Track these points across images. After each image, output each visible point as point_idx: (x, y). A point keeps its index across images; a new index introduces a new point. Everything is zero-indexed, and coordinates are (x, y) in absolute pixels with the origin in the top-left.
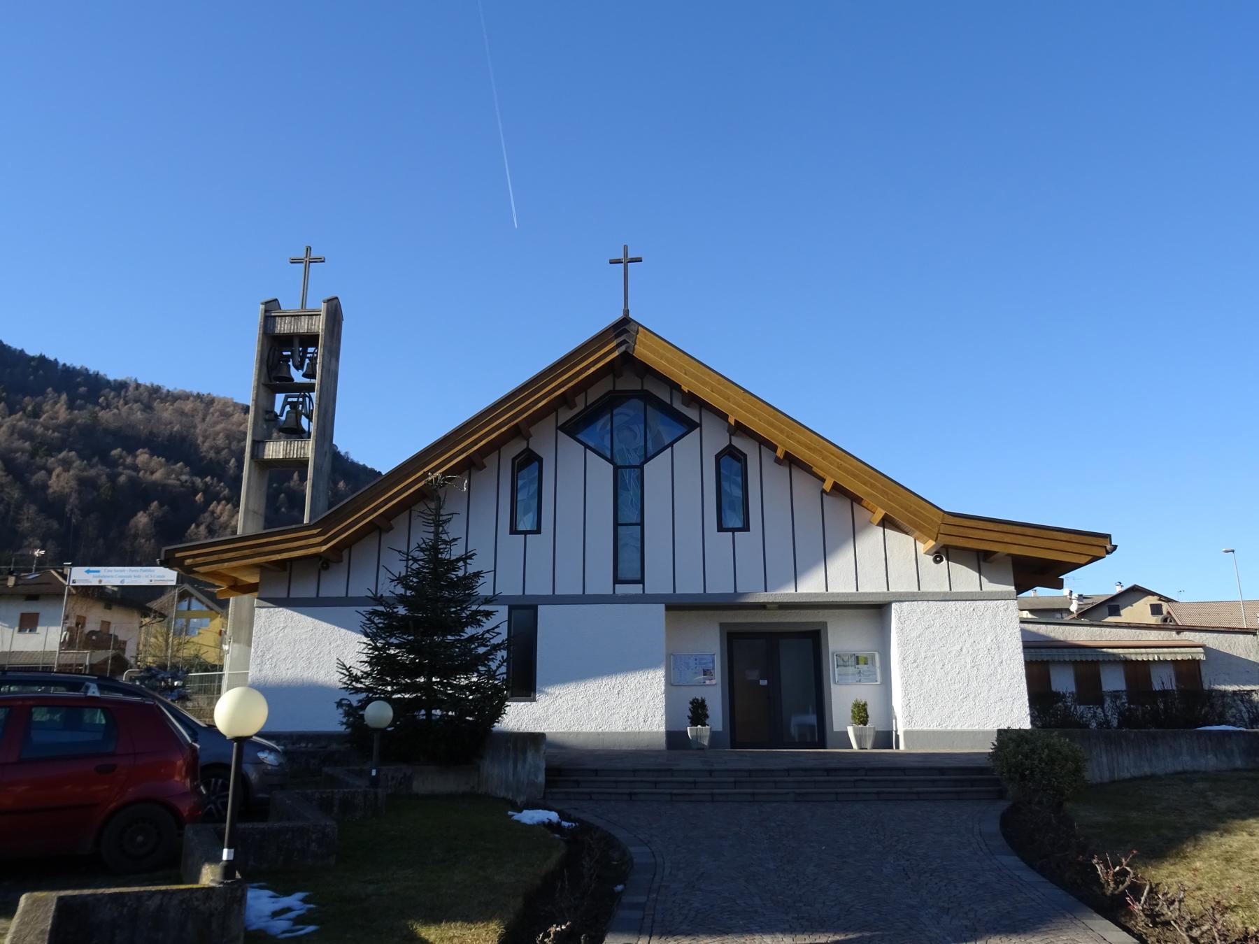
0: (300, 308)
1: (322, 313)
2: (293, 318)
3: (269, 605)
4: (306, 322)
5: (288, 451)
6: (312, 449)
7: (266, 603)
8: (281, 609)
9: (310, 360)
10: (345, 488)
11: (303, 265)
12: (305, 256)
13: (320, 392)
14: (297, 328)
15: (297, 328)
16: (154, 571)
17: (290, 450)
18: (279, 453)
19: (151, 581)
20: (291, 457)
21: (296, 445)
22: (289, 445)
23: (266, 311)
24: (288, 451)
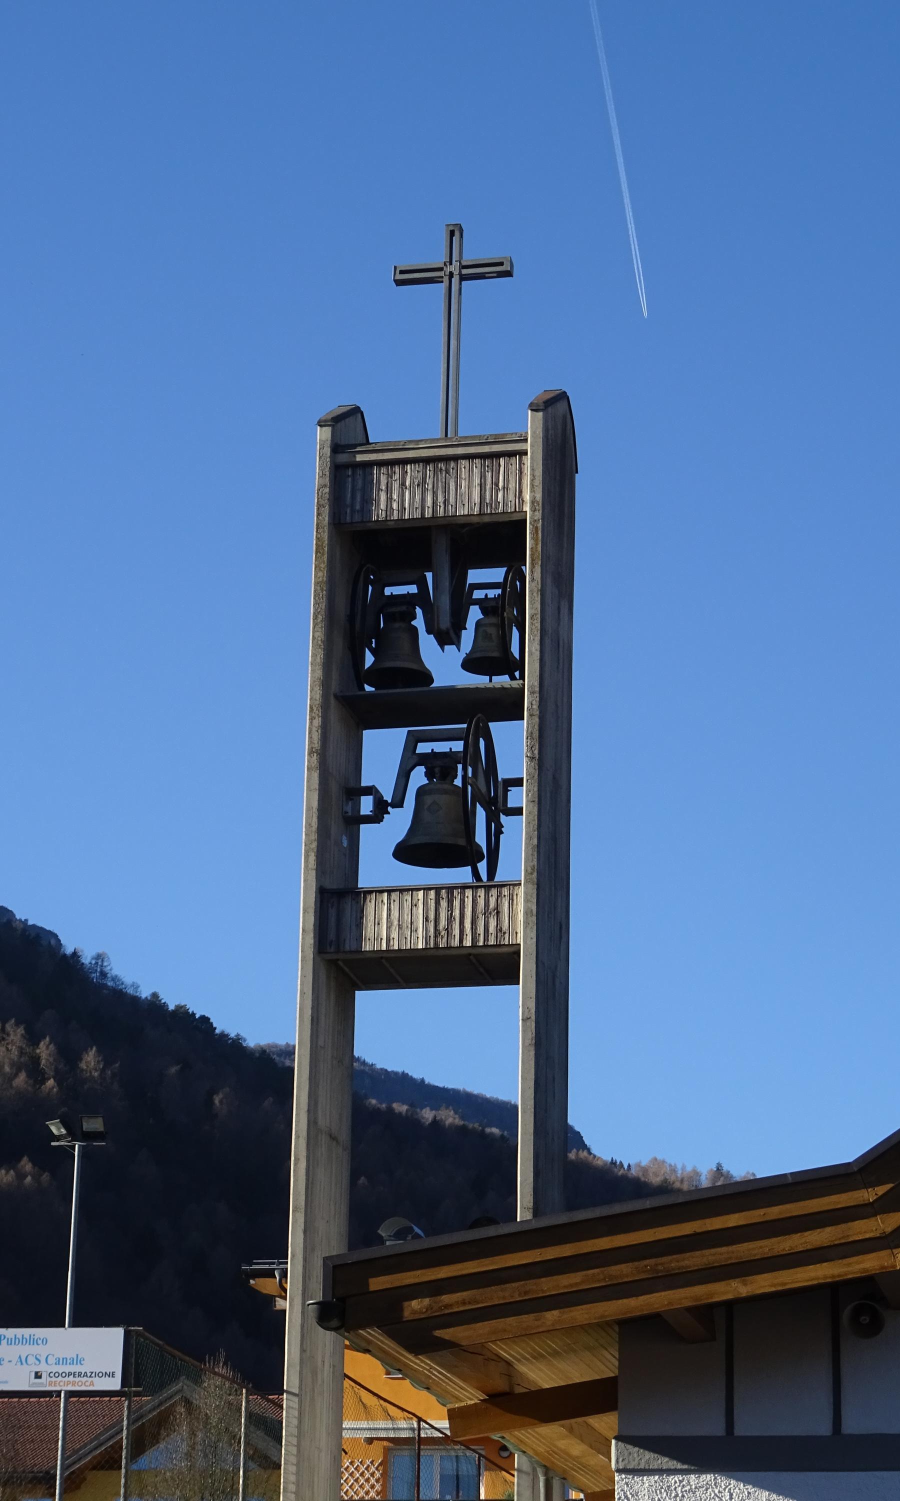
0: (440, 434)
1: (528, 446)
2: (430, 467)
3: (665, 1462)
4: (477, 481)
5: (443, 923)
6: (526, 913)
7: (648, 1455)
8: (708, 1477)
9: (484, 611)
10: (103, 1071)
11: (442, 287)
12: (445, 258)
13: (542, 718)
14: (446, 502)
15: (446, 502)
16: (45, 1341)
17: (450, 919)
18: (414, 930)
19: (38, 1376)
20: (456, 943)
21: (469, 902)
22: (444, 904)
23: (336, 448)
24: (443, 923)
